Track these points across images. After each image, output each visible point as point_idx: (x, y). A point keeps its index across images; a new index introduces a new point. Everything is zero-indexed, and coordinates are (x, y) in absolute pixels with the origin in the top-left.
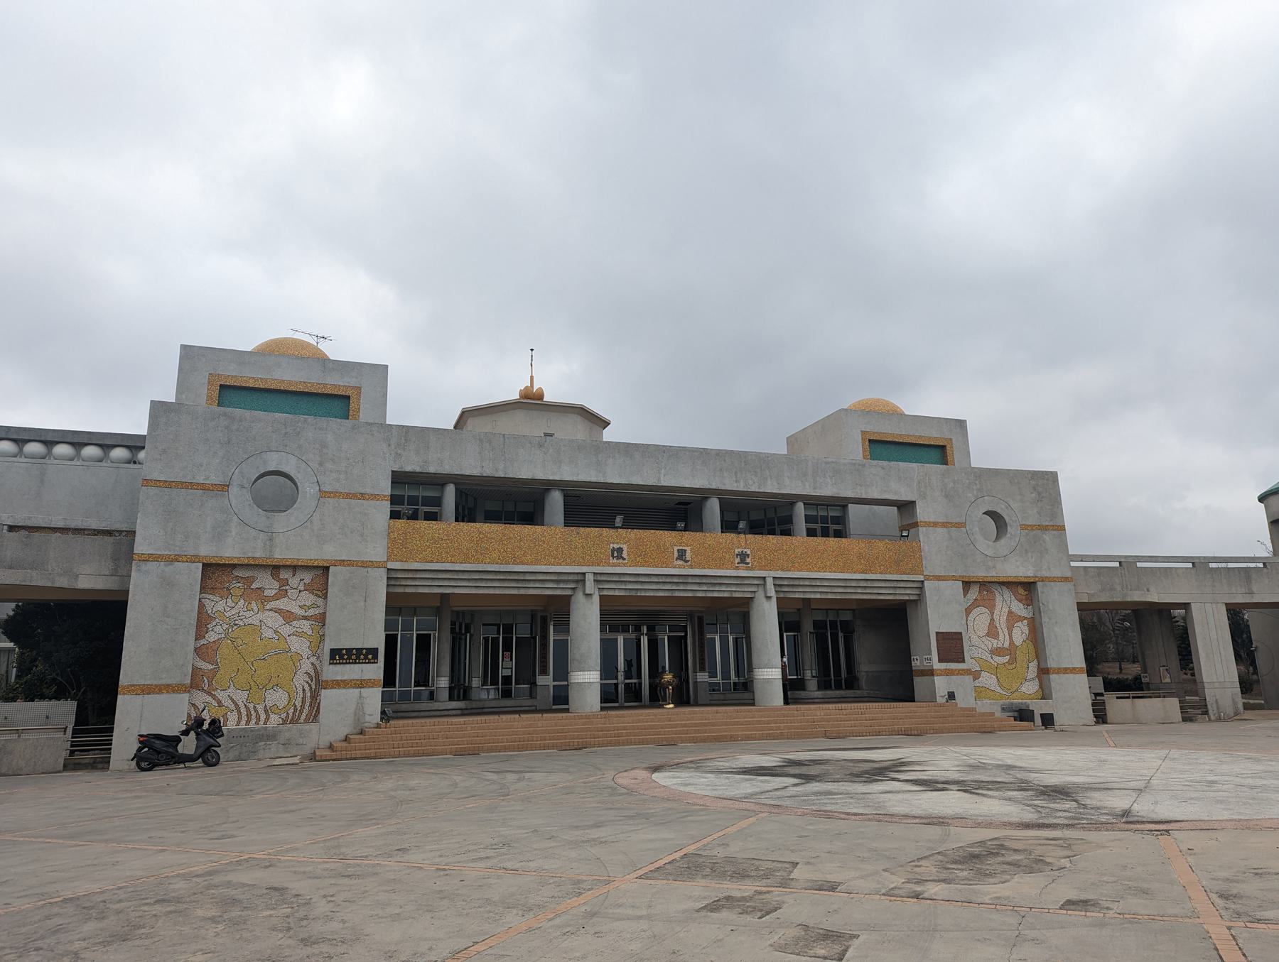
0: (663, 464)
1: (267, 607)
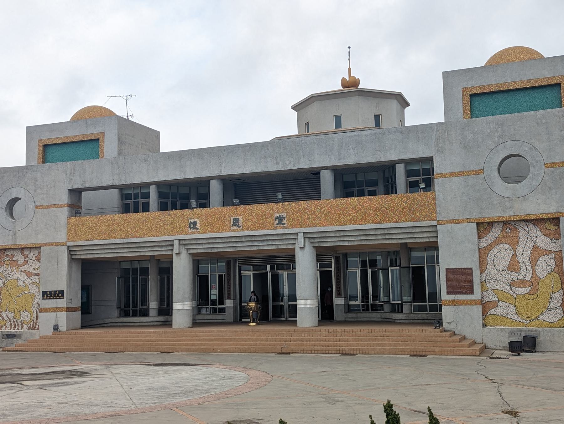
0: (224, 159)
1: (19, 270)
